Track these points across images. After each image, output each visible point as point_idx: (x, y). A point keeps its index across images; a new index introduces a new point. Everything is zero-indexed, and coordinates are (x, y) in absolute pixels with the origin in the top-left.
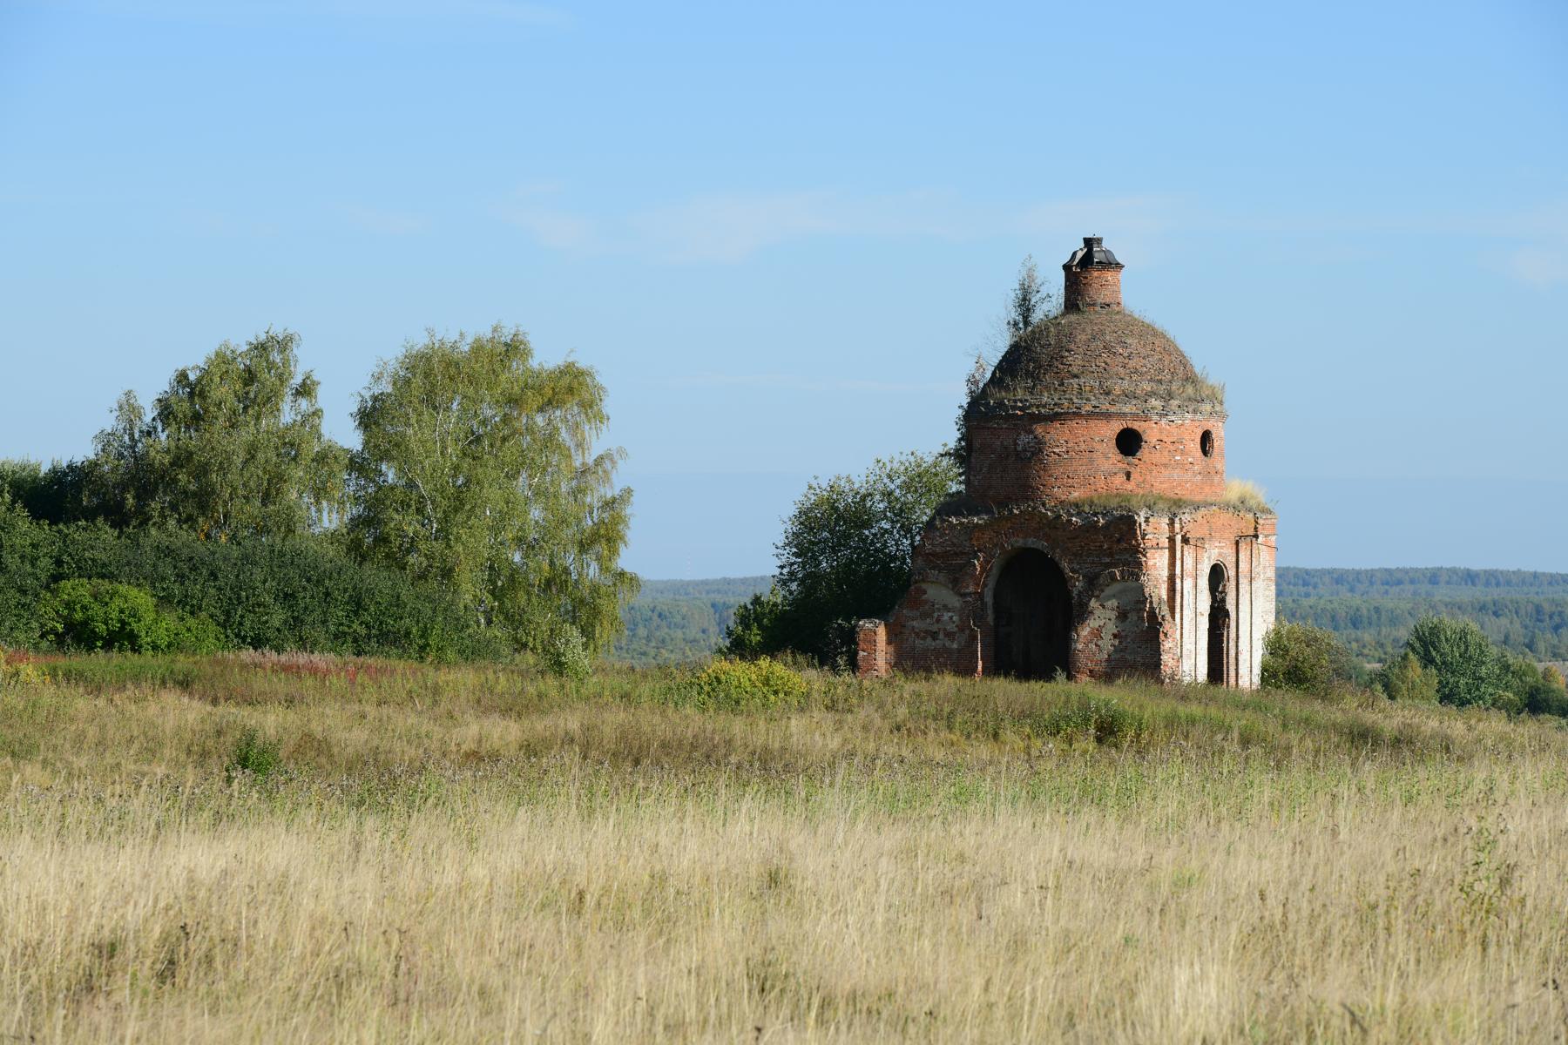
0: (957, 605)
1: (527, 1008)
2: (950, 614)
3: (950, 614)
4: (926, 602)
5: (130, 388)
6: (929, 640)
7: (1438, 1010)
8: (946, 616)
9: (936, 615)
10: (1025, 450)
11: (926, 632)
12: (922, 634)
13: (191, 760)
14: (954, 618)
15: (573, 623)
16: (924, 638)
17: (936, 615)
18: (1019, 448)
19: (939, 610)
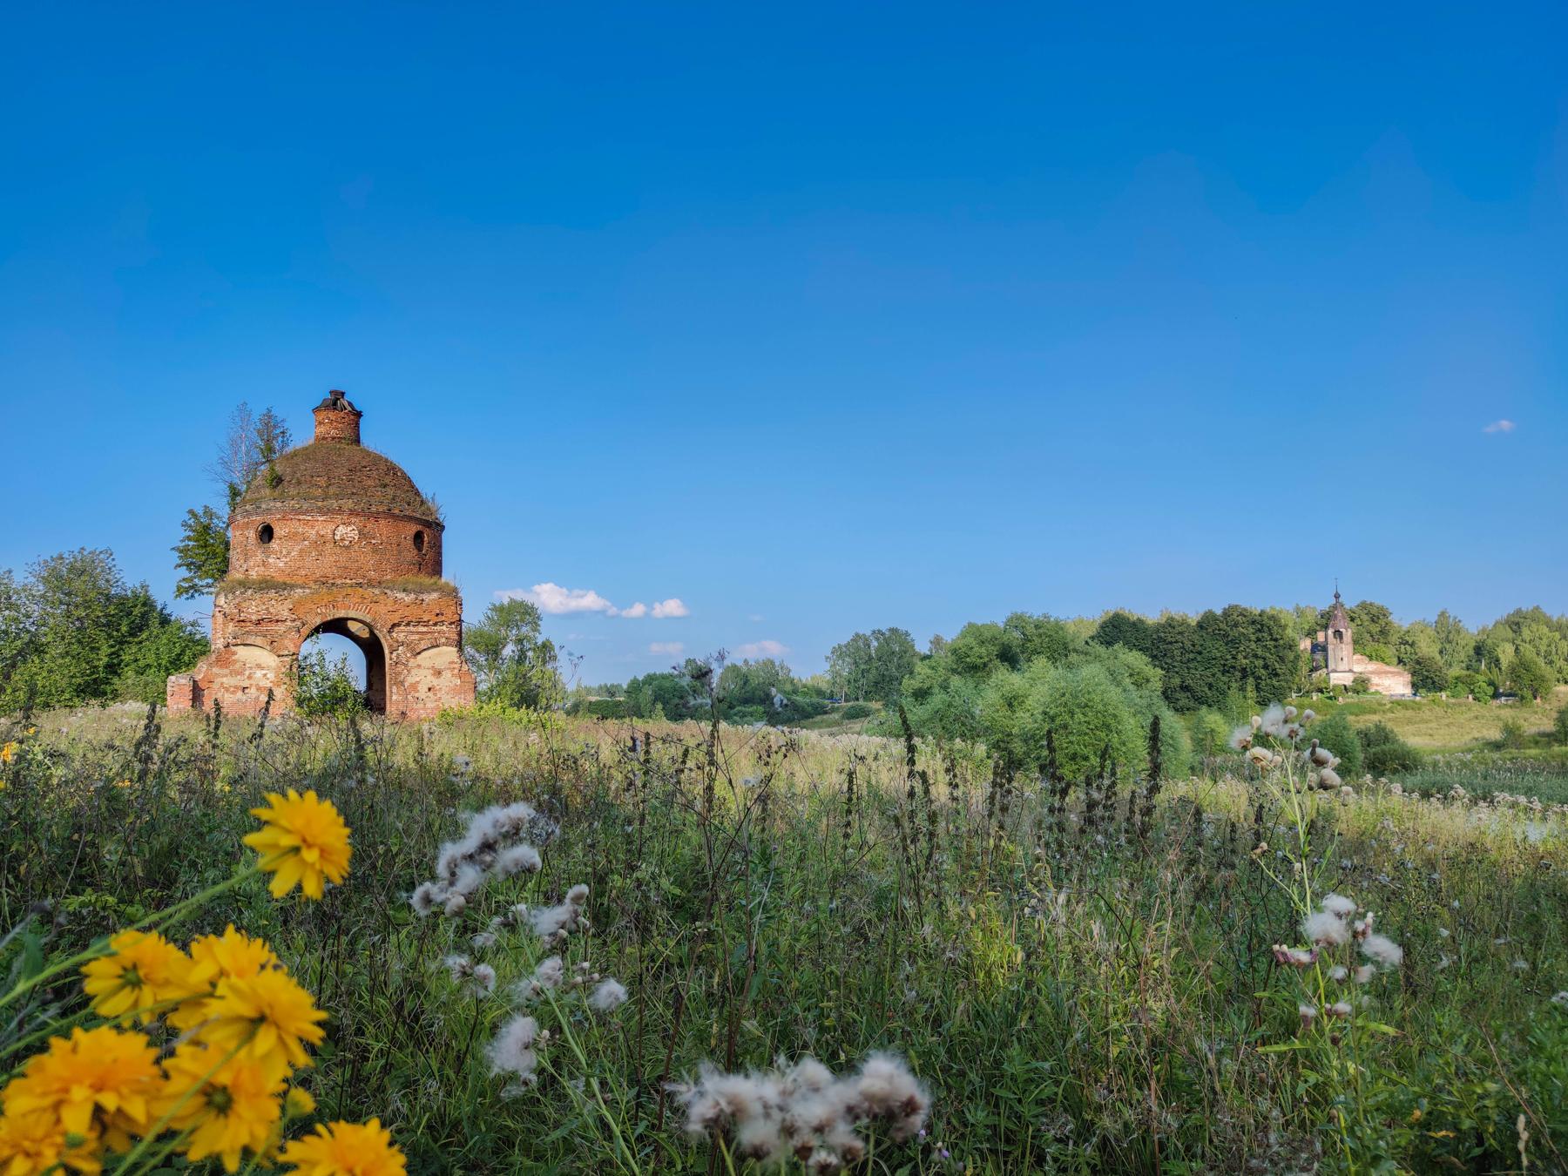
0: (273, 664)
1: (730, 796)
2: (264, 672)
3: (264, 672)
4: (236, 661)
5: (1441, 610)
6: (240, 693)
7: (1116, 658)
8: (259, 674)
9: (247, 673)
10: (343, 540)
11: (236, 687)
12: (232, 689)
13: (1372, 811)
14: (268, 676)
15: (399, 889)
16: (234, 693)
17: (247, 673)
18: (337, 538)
19: (251, 668)
